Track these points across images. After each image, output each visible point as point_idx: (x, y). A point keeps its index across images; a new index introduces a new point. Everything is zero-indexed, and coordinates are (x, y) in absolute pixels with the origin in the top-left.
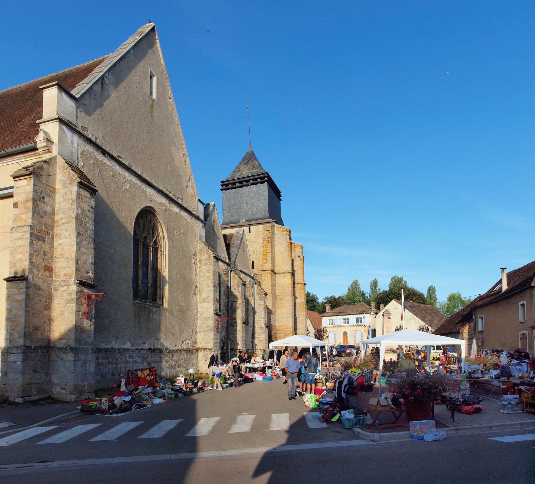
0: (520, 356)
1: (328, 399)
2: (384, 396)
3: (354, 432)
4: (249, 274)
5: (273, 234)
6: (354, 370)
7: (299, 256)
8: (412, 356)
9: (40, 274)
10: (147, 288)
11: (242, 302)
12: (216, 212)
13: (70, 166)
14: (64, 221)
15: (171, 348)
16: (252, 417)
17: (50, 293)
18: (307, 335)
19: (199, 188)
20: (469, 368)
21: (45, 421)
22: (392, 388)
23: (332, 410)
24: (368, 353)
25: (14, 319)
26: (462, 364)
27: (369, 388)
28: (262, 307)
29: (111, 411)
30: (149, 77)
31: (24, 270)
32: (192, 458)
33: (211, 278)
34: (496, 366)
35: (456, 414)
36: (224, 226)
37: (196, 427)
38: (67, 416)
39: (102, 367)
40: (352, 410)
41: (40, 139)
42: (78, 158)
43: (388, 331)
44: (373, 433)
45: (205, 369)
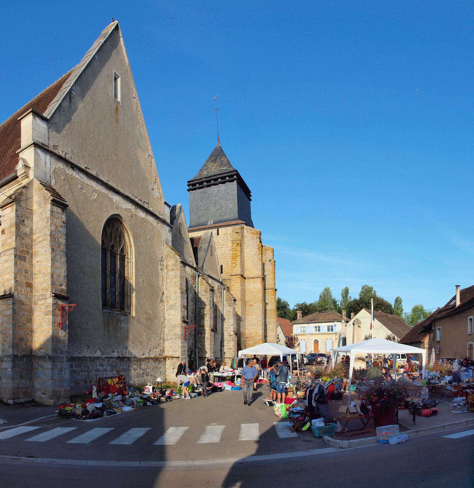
0: (468, 363)
1: (299, 408)
2: (353, 403)
3: (324, 441)
4: (218, 279)
5: (242, 236)
6: (325, 378)
7: (270, 260)
8: (380, 364)
9: (23, 291)
10: (116, 297)
11: (210, 308)
12: (182, 214)
13: (44, 186)
14: (40, 239)
15: (139, 357)
16: (222, 427)
17: (31, 307)
18: (278, 343)
19: (165, 189)
20: (429, 375)
21: (30, 422)
22: (361, 396)
23: (302, 419)
24: (338, 362)
25: (5, 332)
26: (423, 371)
27: (339, 396)
28: (231, 314)
29: (84, 417)
30: (114, 80)
31: (11, 288)
32: (161, 467)
33: (179, 284)
34: (450, 373)
35: (417, 418)
36: (191, 229)
37: (164, 436)
38: (48, 418)
39: (75, 375)
40: (322, 419)
41: (20, 168)
42: (51, 177)
43: (358, 340)
44: (342, 440)
45: (173, 378)
